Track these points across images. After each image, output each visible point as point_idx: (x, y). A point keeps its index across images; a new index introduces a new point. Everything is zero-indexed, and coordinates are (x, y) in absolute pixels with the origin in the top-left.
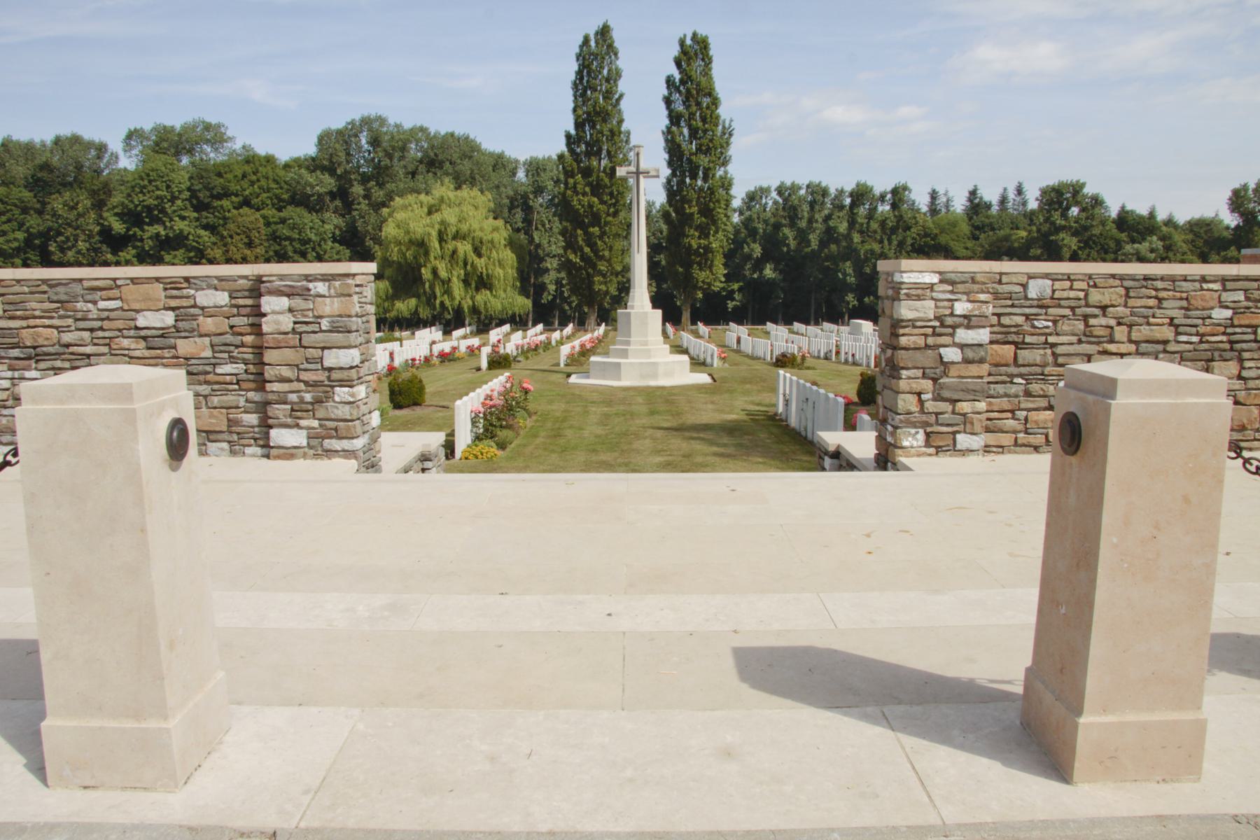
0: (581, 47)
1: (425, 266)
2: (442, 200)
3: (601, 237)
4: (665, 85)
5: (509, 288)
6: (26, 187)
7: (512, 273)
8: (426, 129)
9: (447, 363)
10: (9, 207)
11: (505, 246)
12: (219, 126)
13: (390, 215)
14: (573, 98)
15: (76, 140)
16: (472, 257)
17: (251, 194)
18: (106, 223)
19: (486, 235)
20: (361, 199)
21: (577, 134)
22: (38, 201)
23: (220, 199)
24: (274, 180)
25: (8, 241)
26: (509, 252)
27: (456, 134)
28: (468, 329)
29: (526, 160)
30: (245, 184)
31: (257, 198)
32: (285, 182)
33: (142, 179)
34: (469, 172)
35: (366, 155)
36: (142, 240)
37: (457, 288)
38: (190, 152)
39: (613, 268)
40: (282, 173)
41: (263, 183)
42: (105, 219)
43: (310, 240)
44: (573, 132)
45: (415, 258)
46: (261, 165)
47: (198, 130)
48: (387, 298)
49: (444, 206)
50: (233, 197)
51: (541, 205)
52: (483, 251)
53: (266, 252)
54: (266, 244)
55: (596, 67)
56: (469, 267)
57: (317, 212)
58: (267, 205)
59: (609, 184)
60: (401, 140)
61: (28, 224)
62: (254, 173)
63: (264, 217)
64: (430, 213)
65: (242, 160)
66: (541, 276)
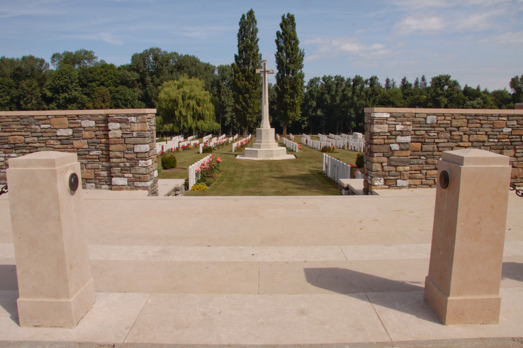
0: (241, 19)
1: (176, 110)
2: (183, 83)
3: (249, 98)
4: (276, 35)
5: (211, 119)
6: (11, 77)
7: (212, 113)
8: (177, 53)
9: (185, 151)
10: (3, 86)
12: (91, 52)
13: (162, 89)
14: (238, 41)
15: (31, 58)
16: (196, 106)
17: (104, 80)
18: (44, 92)
19: (202, 97)
21: (239, 56)
22: (16, 83)
24: (114, 75)
25: (3, 100)
26: (211, 104)
27: (190, 55)
29: (219, 66)
30: (102, 76)
31: (107, 82)
33: (59, 74)
34: (195, 71)
35: (152, 64)
36: (59, 99)
38: (79, 63)
39: (254, 111)
40: (117, 72)
41: (109, 76)
42: (44, 91)
43: (129, 99)
44: (238, 55)
45: (172, 107)
46: (108, 68)
48: (161, 124)
49: (184, 86)
51: (225, 85)
53: (111, 104)
54: (110, 101)
56: (195, 111)
57: (132, 88)
58: (111, 85)
59: (253, 76)
60: (166, 58)
62: (106, 72)
63: (110, 90)
65: (100, 66)
66: (225, 114)
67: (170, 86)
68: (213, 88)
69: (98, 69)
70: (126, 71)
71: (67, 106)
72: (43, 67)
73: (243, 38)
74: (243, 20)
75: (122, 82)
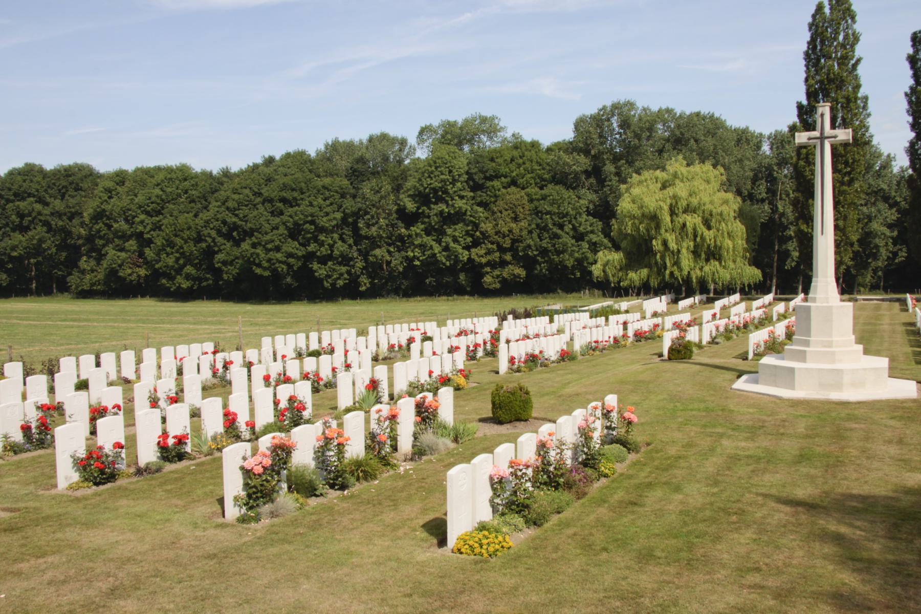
0: (814, 16)
1: (656, 238)
2: (675, 176)
4: (910, 43)
5: (738, 259)
6: (346, 176)
7: (741, 243)
8: (672, 110)
9: (643, 342)
10: (332, 193)
11: (735, 218)
12: (493, 118)
13: (627, 190)
14: (805, 69)
15: (384, 137)
16: (702, 229)
17: (517, 175)
18: (402, 203)
19: (715, 208)
20: (612, 176)
21: (809, 104)
22: (354, 187)
23: (492, 180)
24: (537, 162)
25: (330, 220)
26: (739, 223)
27: (702, 113)
28: (697, 298)
29: (771, 134)
30: (513, 166)
31: (523, 178)
32: (548, 164)
33: (431, 166)
34: (712, 148)
35: (617, 136)
36: (429, 217)
37: (686, 261)
38: (470, 141)
39: (848, 238)
40: (544, 156)
41: (528, 165)
42: (401, 200)
43: (567, 214)
44: (805, 102)
45: (647, 230)
46: (527, 150)
47: (477, 122)
48: (621, 269)
49: (677, 181)
50: (503, 178)
51: (785, 176)
52: (713, 224)
53: (529, 225)
54: (529, 218)
55: (831, 33)
56: (698, 239)
57: (574, 189)
58: (531, 184)
59: (843, 152)
60: (648, 121)
61: (344, 206)
62: (521, 157)
63: (528, 195)
64: (664, 187)
65: (511, 147)
66: (785, 243)
67: (645, 184)
68: (757, 183)
69: (506, 153)
70: (561, 153)
71: (445, 230)
72: (405, 153)
73: (818, 60)
74: (818, 16)
75: (554, 177)
